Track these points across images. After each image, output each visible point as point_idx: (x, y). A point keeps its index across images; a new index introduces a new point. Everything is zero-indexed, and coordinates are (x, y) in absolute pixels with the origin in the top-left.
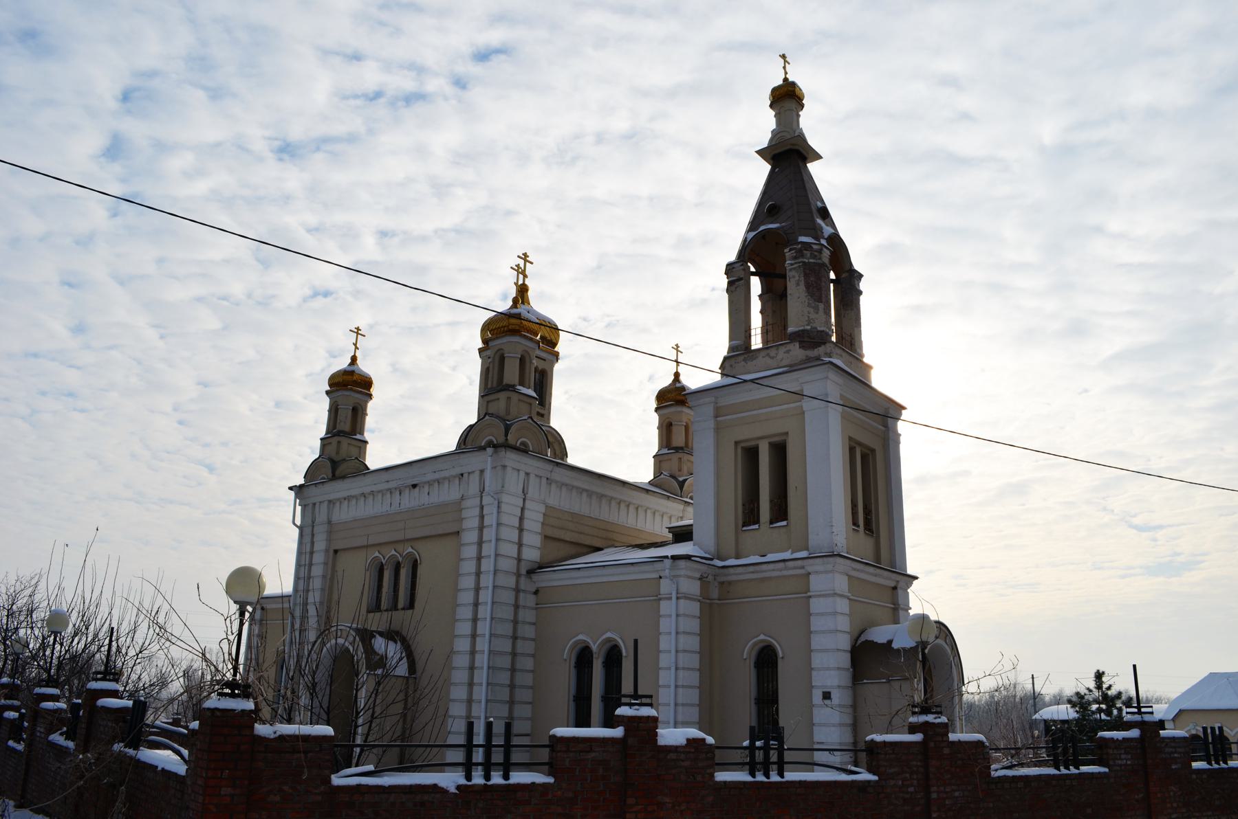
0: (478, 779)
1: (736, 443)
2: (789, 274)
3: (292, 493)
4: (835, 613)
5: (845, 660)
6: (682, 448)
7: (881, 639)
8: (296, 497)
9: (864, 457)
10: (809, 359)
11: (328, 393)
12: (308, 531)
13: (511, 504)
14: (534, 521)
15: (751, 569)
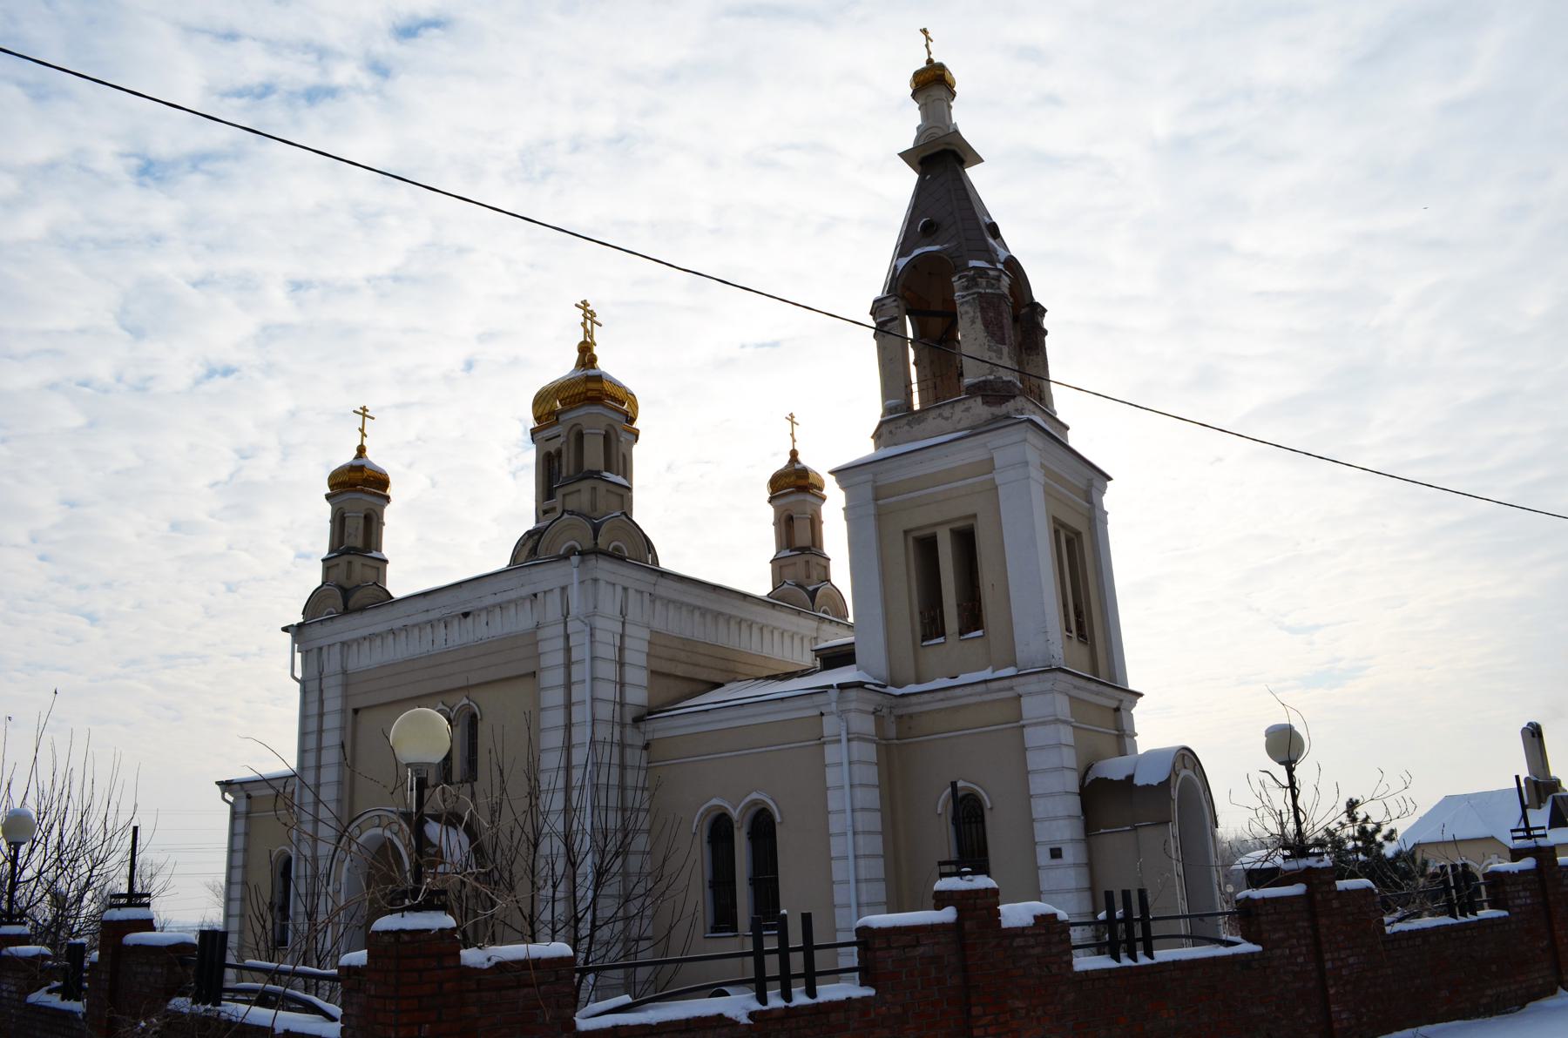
0: (775, 1002)
1: (906, 532)
2: (960, 310)
3: (288, 636)
4: (1059, 745)
5: (1073, 805)
6: (808, 548)
7: (1118, 775)
8: (294, 641)
9: (1069, 542)
10: (995, 419)
11: (328, 497)
12: (314, 685)
13: (608, 628)
14: (637, 654)
15: (940, 695)
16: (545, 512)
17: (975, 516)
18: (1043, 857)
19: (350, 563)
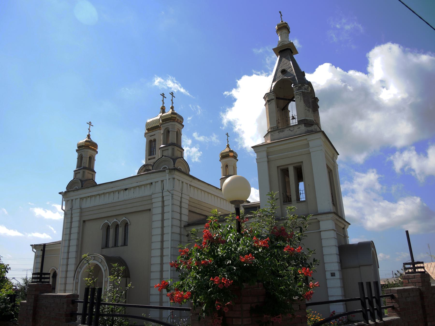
1: (278, 167)
14: (185, 205)
16: (149, 159)
17: (302, 162)
18: (328, 275)
19: (84, 172)
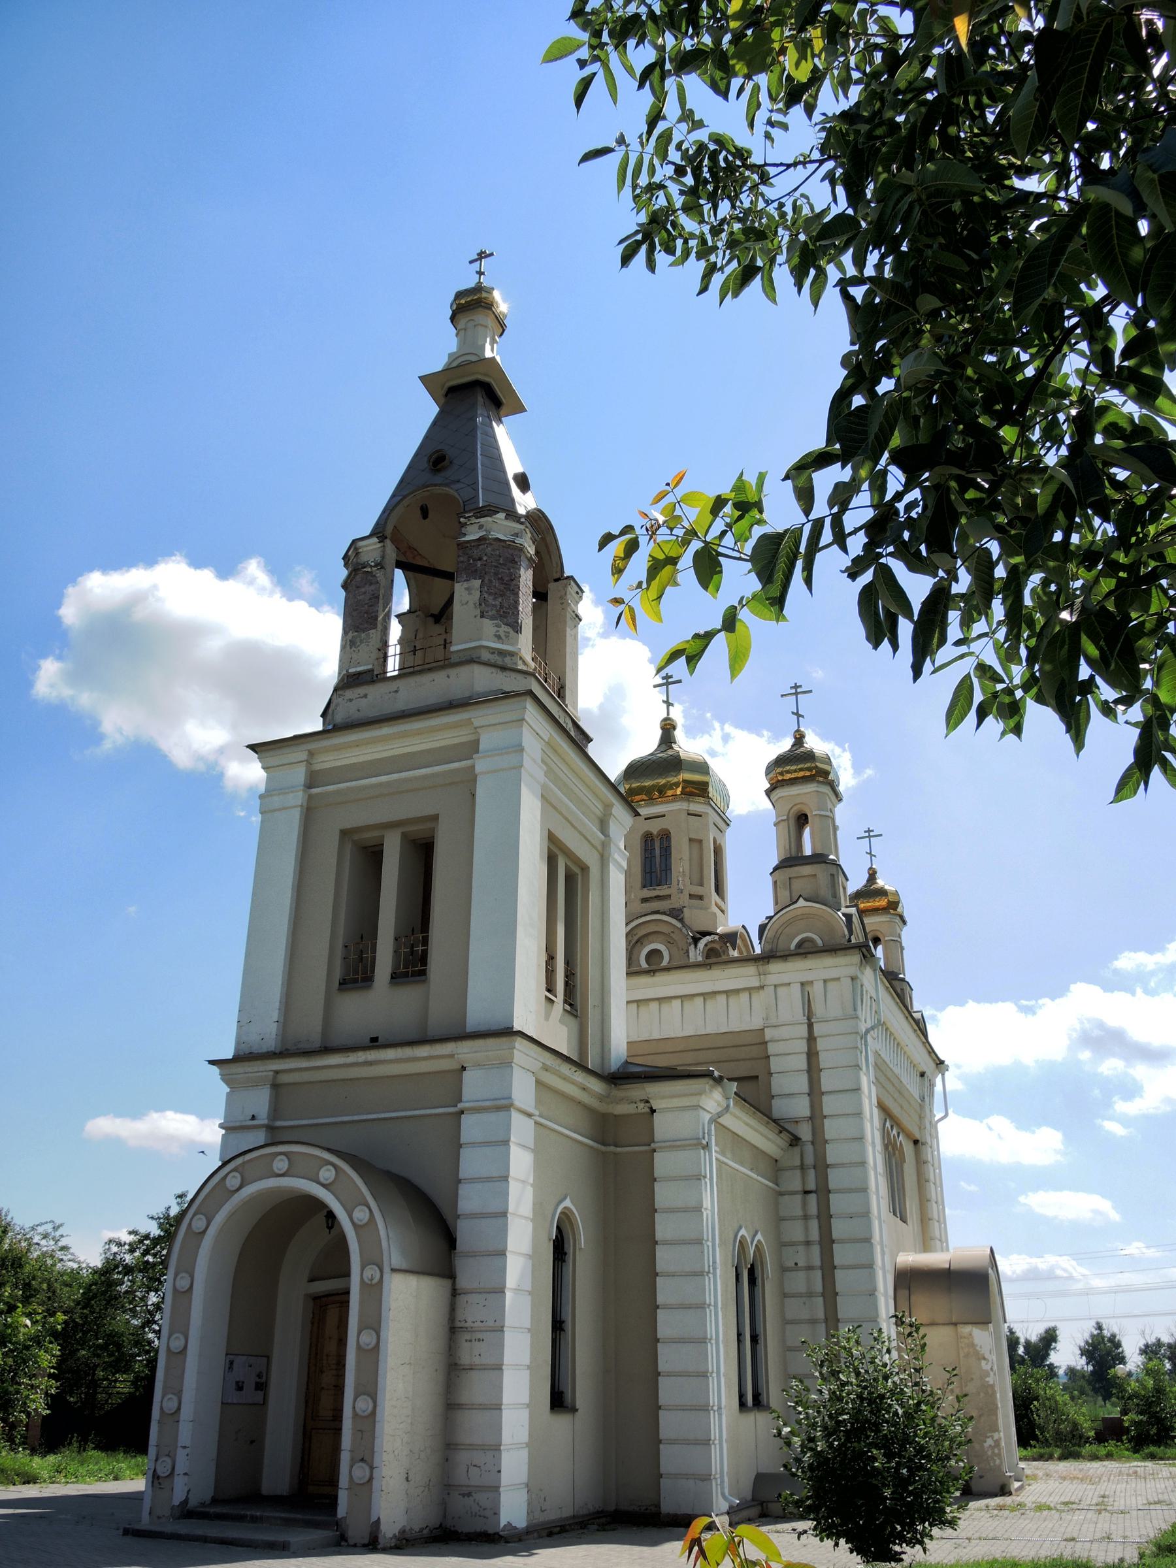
9: (570, 879)
17: (435, 818)
